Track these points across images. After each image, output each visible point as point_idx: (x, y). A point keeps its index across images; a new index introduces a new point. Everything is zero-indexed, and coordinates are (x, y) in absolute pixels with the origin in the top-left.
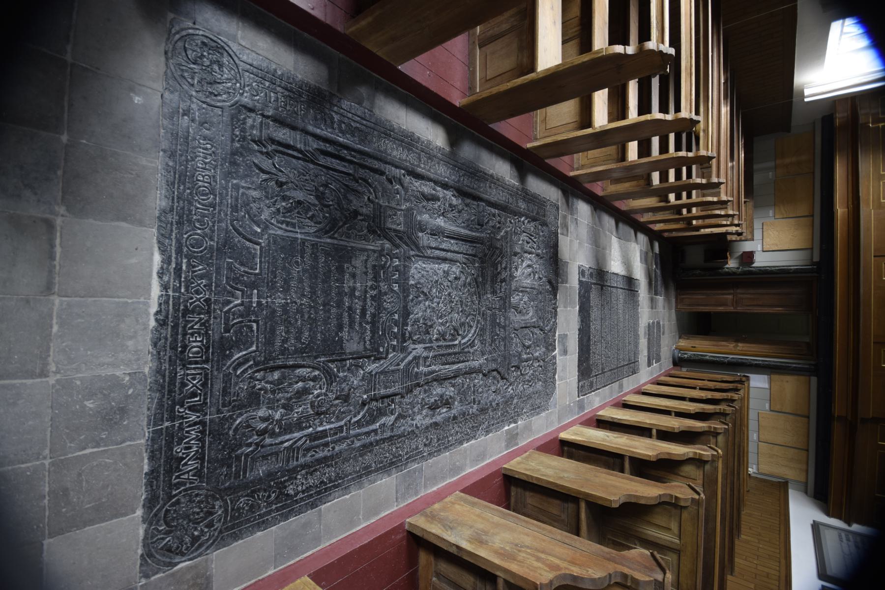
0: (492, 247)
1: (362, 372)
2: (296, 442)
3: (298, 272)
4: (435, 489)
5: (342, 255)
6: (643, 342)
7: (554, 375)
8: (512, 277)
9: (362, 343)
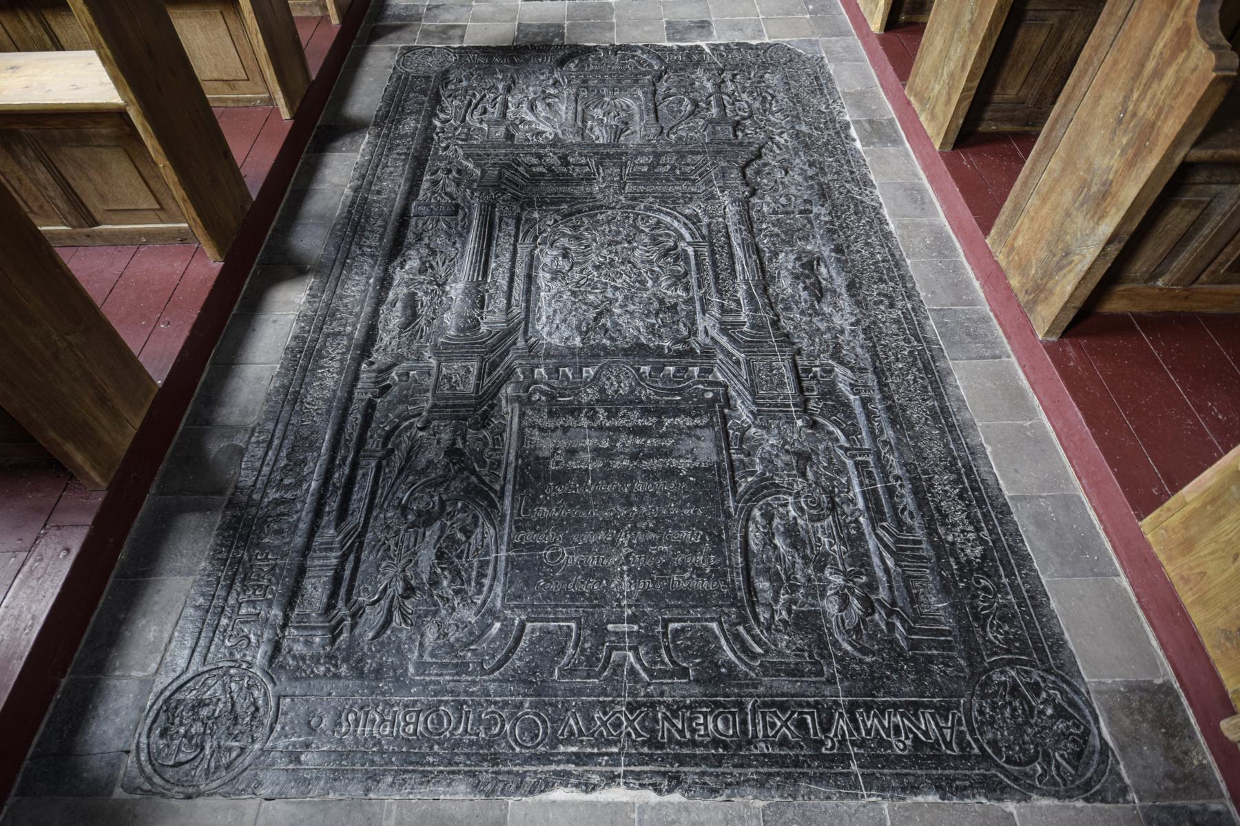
0: (499, 185)
1: (753, 430)
2: (886, 546)
3: (570, 553)
4: (977, 284)
5: (534, 475)
7: (750, 47)
8: (556, 143)
9: (698, 432)
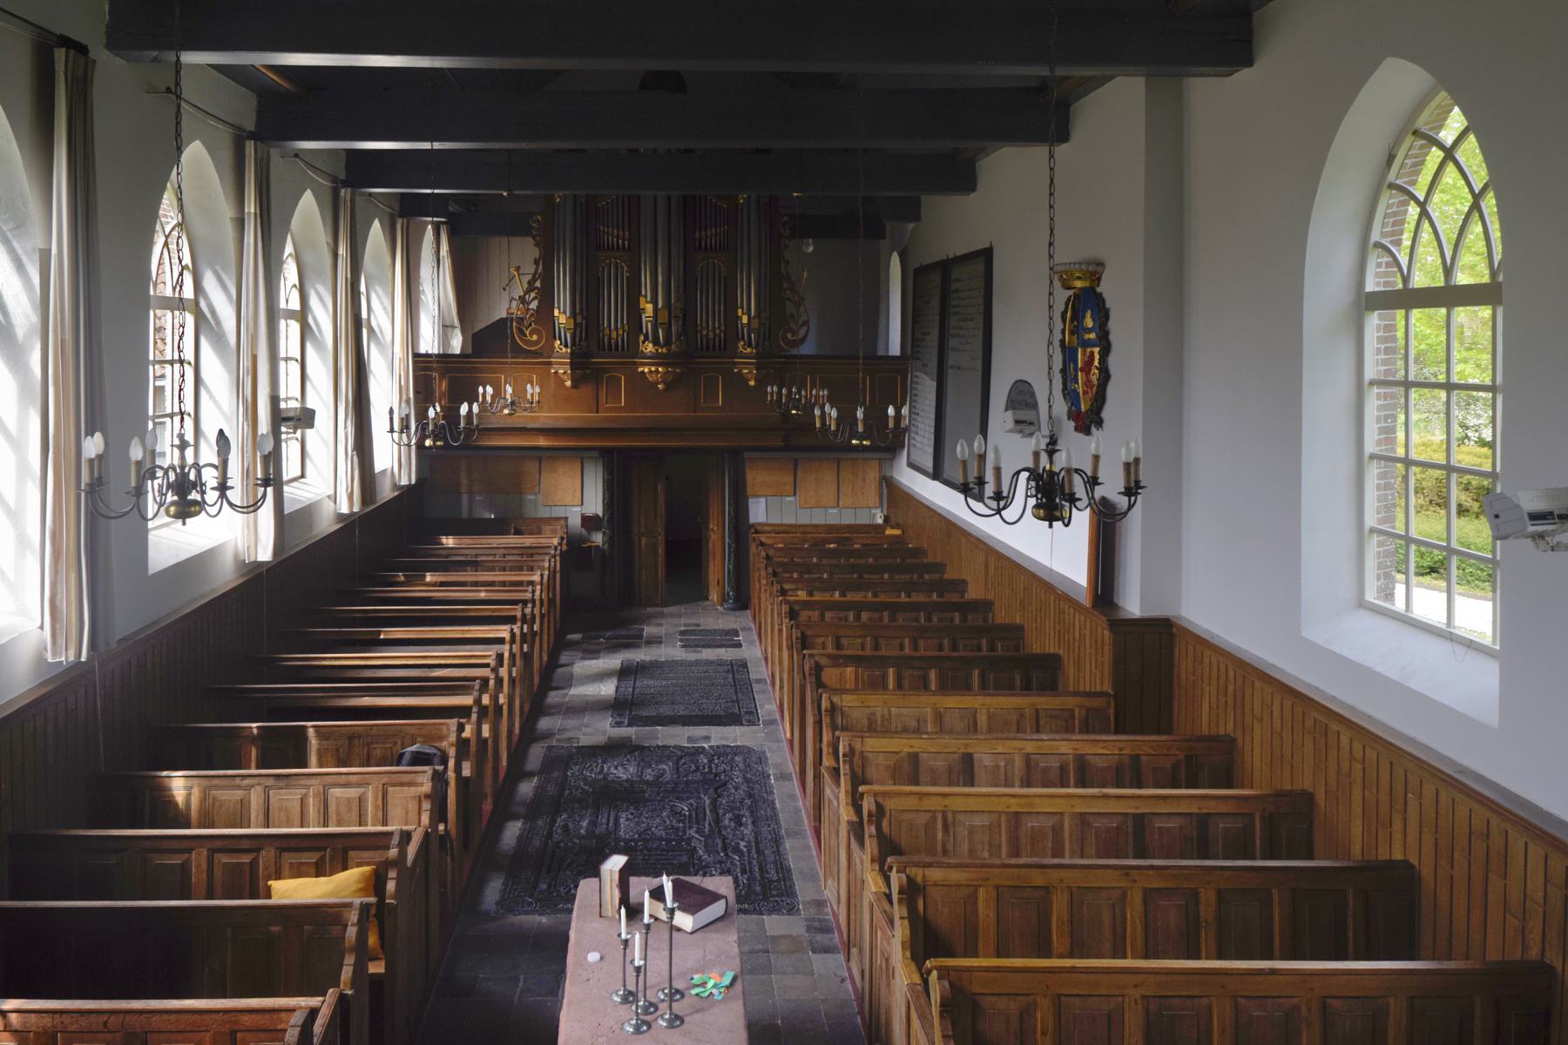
6: (708, 654)
